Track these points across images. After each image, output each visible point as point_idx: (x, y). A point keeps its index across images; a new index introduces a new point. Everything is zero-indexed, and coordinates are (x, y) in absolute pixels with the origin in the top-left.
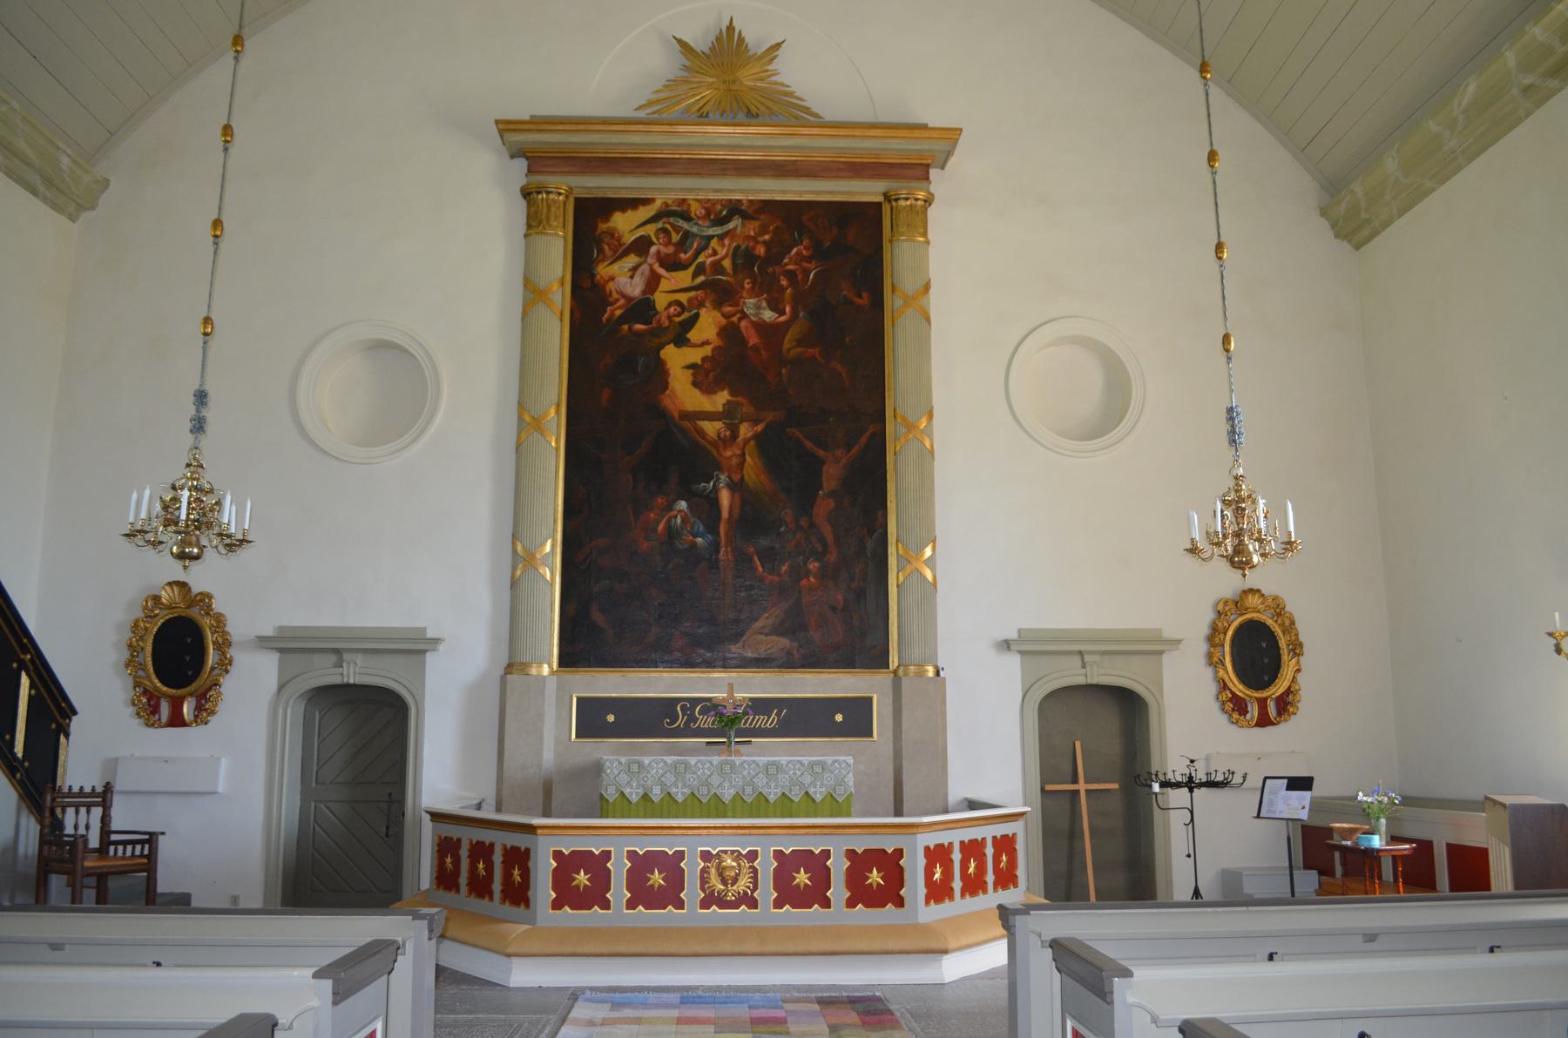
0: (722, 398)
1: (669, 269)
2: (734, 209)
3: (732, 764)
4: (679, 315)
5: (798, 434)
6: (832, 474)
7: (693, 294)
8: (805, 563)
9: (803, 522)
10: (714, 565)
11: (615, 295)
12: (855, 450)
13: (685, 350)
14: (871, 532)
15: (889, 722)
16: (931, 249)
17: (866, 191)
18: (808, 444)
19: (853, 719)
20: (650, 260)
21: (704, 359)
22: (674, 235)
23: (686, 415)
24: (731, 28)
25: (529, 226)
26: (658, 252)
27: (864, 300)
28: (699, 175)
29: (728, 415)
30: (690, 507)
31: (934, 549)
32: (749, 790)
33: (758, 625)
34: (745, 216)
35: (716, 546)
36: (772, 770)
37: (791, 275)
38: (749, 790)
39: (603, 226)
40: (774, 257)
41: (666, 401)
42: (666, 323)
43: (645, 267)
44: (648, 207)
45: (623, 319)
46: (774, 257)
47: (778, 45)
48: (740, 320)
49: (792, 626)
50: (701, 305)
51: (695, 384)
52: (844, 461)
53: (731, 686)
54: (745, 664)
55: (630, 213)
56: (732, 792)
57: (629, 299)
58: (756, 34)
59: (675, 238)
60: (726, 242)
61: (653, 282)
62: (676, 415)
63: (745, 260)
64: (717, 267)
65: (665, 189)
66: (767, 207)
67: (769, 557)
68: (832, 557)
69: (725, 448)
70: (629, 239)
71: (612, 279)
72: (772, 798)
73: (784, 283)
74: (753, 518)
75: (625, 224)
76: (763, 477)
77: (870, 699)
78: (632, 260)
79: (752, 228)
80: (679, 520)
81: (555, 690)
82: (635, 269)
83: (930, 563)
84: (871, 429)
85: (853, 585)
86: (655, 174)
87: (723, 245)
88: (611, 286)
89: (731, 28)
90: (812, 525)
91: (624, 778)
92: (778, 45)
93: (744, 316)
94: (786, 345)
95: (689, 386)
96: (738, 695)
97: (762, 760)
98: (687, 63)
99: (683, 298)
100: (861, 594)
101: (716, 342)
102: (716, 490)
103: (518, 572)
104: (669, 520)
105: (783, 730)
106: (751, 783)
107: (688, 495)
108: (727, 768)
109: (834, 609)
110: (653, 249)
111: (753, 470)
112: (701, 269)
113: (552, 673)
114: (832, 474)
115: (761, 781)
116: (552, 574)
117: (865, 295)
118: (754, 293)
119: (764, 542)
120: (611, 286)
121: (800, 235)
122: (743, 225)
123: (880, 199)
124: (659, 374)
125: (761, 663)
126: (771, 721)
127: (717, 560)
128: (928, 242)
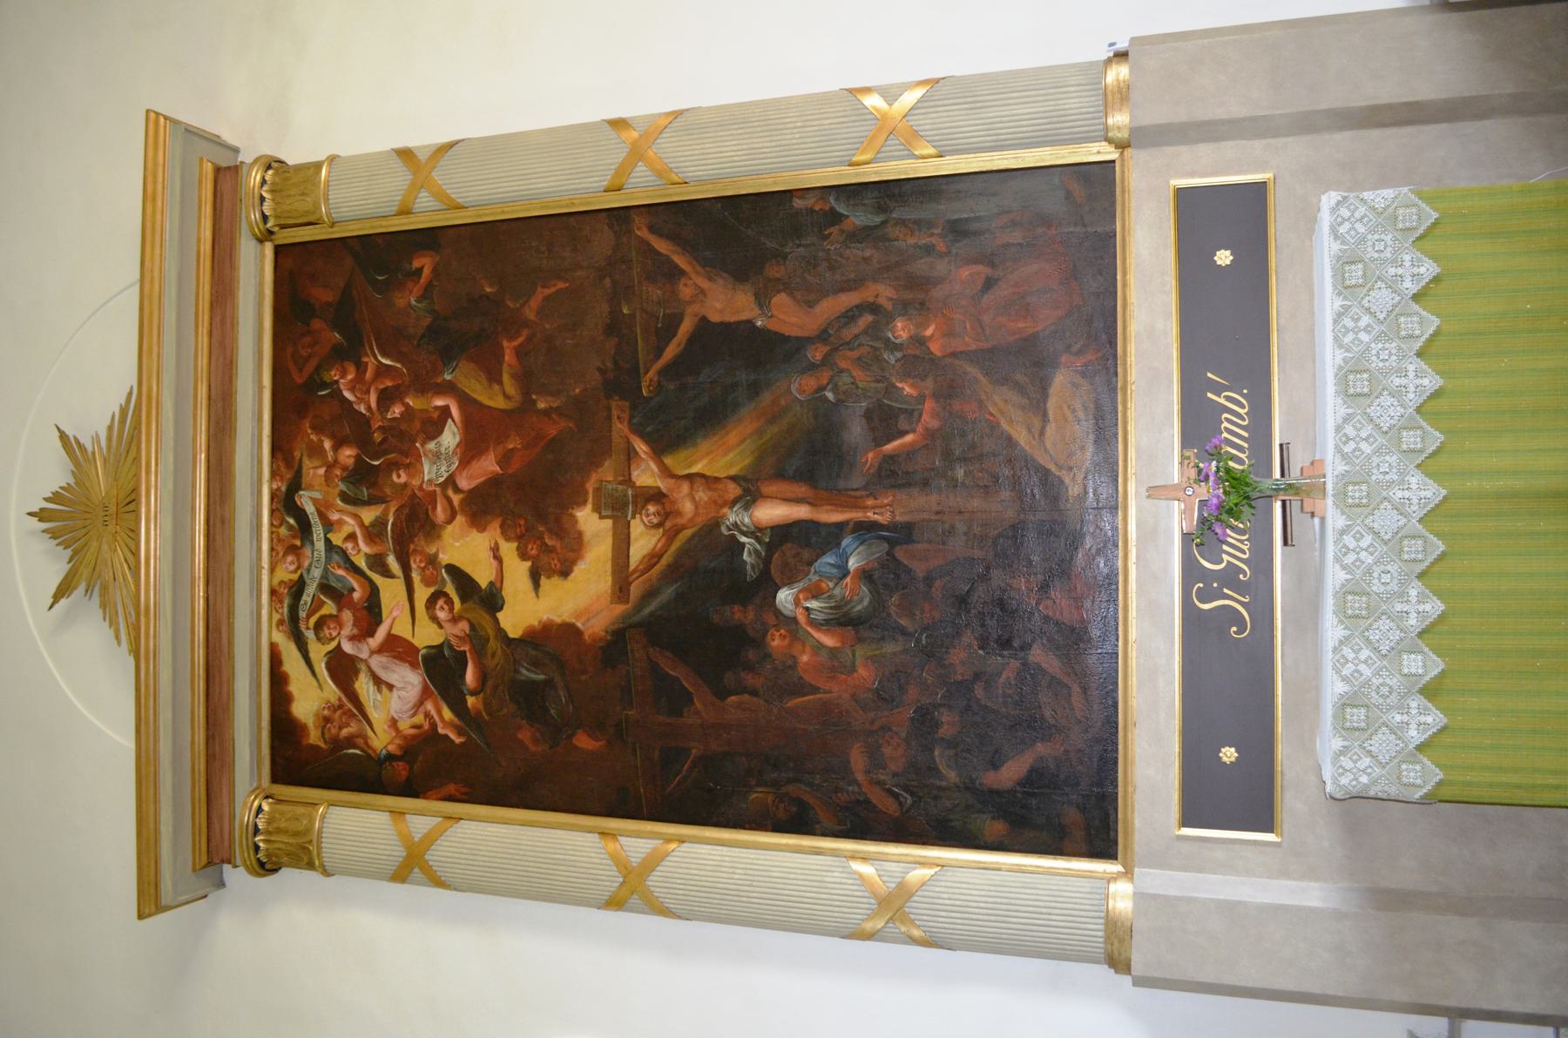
0: (590, 521)
1: (379, 622)
2: (286, 503)
3: (1345, 481)
4: (450, 602)
5: (651, 373)
6: (724, 302)
7: (416, 577)
8: (897, 347)
9: (816, 354)
10: (902, 534)
11: (419, 719)
12: (680, 261)
13: (508, 592)
14: (835, 218)
15: (1230, 149)
16: (343, 152)
17: (255, 272)
18: (671, 351)
19: (1227, 227)
20: (364, 655)
21: (523, 556)
22: (325, 611)
23: (621, 588)
24: (41, 515)
25: (310, 866)
26: (352, 638)
27: (424, 263)
28: (231, 564)
29: (618, 508)
30: (789, 582)
31: (867, 90)
32: (1411, 439)
33: (1021, 437)
34: (295, 485)
35: (865, 529)
36: (1361, 384)
37: (386, 398)
38: (1411, 439)
39: (314, 737)
40: (353, 428)
41: (596, 626)
42: (464, 626)
43: (377, 662)
44: (285, 657)
45: (458, 707)
46: (353, 428)
47: (63, 436)
48: (457, 490)
49: (1027, 365)
50: (432, 561)
51: (565, 573)
52: (705, 284)
53: (1154, 492)
54: (1110, 468)
55: (293, 688)
56: (1415, 479)
57: (425, 694)
58: (54, 474)
59: (329, 608)
60: (334, 517)
61: (397, 648)
62: (620, 609)
63: (363, 482)
64: (374, 533)
65: (255, 624)
66: (280, 448)
67: (885, 421)
68: (884, 292)
69: (679, 513)
70: (332, 691)
71: (394, 723)
72: (1431, 382)
73: (396, 411)
74: (810, 458)
75: (311, 698)
76: (733, 436)
77: (1180, 193)
78: (363, 685)
79: (314, 471)
80: (813, 604)
81: (1168, 869)
82: (378, 681)
83: (890, 94)
84: (644, 233)
85: (941, 246)
86: (231, 643)
87: (341, 522)
88: (405, 726)
89: (41, 515)
90: (823, 336)
91: (1382, 743)
92: (63, 436)
93: (451, 481)
94: (499, 403)
95: (568, 584)
96: (1175, 475)
97: (1332, 408)
98: (82, 588)
99: (422, 594)
100: (957, 230)
101: (493, 533)
102: (756, 532)
103: (916, 933)
104: (812, 623)
105: (1254, 378)
106: (1393, 434)
107: (766, 585)
108: (1356, 493)
109: (989, 284)
110: (348, 648)
111: (721, 456)
112: (378, 563)
113: (1128, 874)
114: (724, 302)
115: (1388, 410)
116: (923, 863)
117: (416, 264)
118: (413, 466)
119: (856, 431)
120: (405, 726)
121: (324, 385)
122: (310, 487)
123: (269, 249)
124: (548, 641)
125: (1106, 426)
126: (1233, 406)
127: (892, 527)
128: (332, 159)
